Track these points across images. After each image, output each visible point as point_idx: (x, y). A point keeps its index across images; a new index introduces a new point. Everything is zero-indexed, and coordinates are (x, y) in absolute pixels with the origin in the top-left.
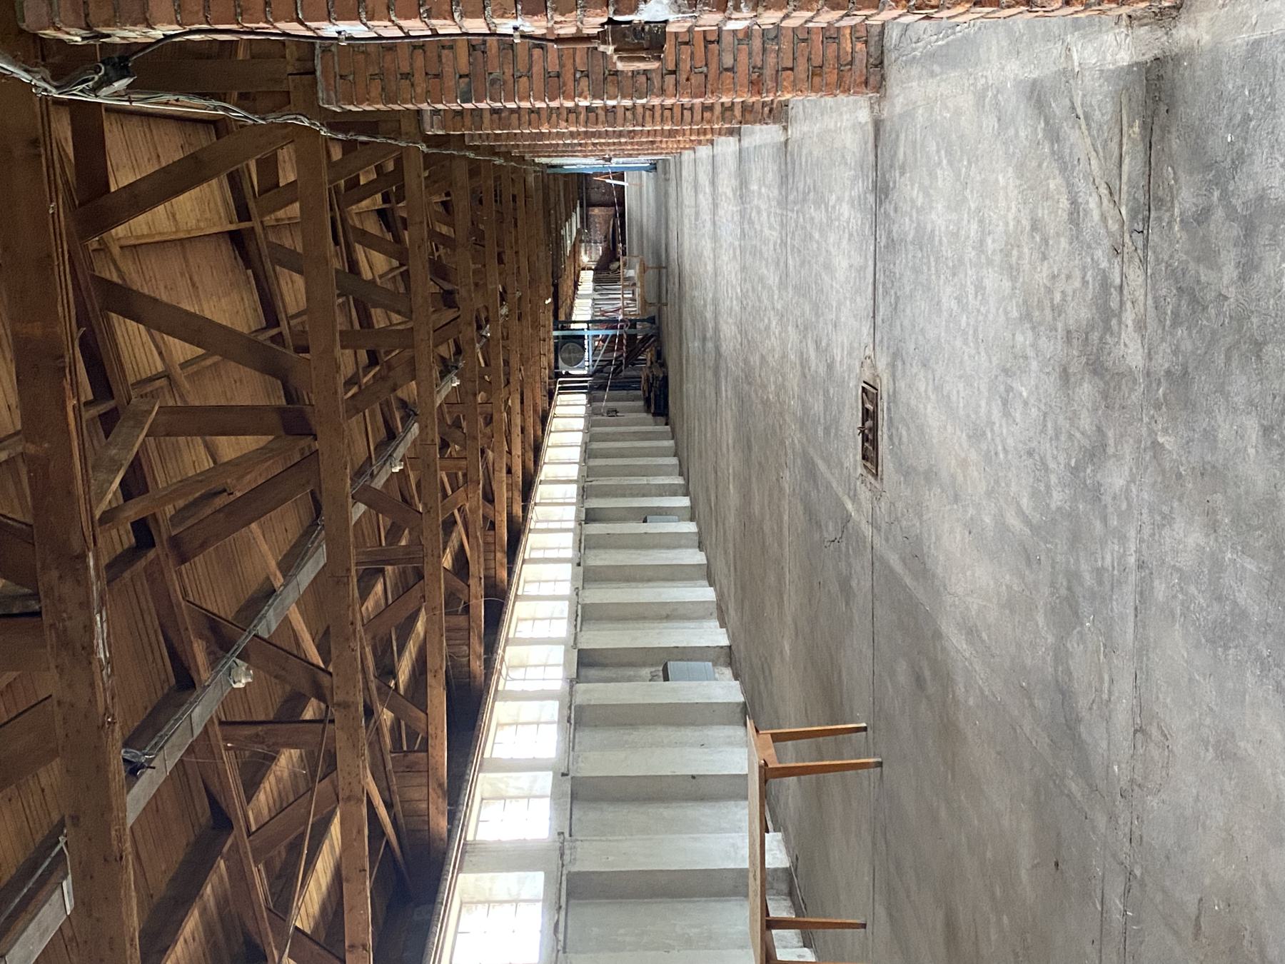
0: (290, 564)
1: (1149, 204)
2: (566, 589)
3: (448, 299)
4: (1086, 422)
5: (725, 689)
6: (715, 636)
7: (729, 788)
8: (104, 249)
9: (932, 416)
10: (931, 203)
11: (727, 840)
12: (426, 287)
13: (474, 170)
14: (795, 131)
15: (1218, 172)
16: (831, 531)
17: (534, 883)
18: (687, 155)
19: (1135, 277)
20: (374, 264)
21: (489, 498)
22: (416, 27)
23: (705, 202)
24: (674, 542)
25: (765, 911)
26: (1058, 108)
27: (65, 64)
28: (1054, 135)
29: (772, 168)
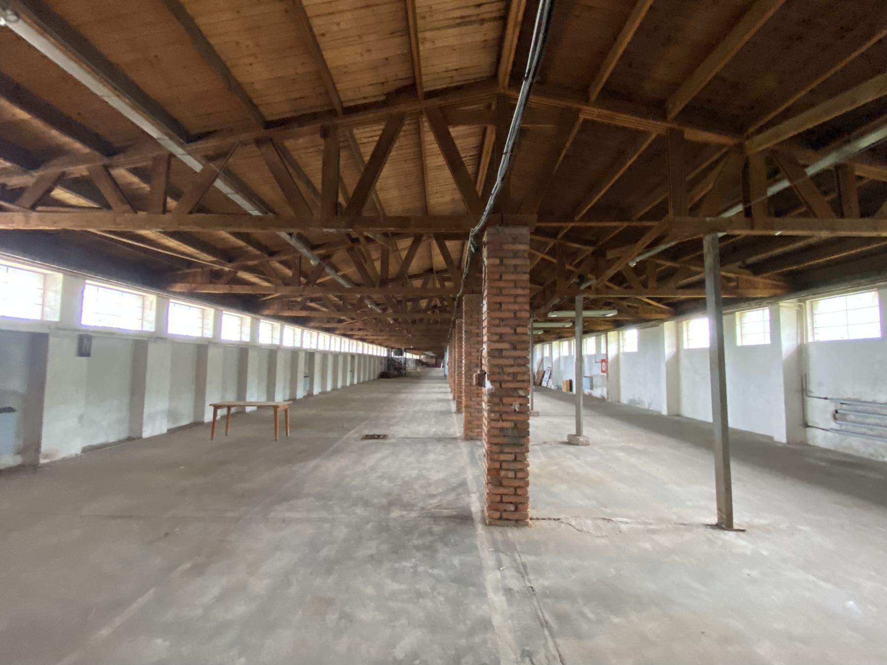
0: (344, 277)
1: (435, 518)
2: (332, 349)
3: (414, 322)
4: (375, 501)
5: (300, 394)
6: (317, 390)
7: (271, 394)
8: (430, 237)
9: (378, 455)
10: (436, 454)
11: (255, 395)
12: (417, 316)
13: (447, 330)
14: (454, 416)
15: (443, 538)
16: (346, 425)
17: (246, 338)
18: (448, 385)
19: (413, 514)
20: (424, 303)
21: (360, 330)
22: (485, 324)
23: (436, 390)
24: (344, 379)
25: (233, 406)
26: (460, 490)
27: (478, 237)
28: (453, 489)
29: (443, 409)
